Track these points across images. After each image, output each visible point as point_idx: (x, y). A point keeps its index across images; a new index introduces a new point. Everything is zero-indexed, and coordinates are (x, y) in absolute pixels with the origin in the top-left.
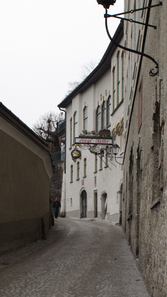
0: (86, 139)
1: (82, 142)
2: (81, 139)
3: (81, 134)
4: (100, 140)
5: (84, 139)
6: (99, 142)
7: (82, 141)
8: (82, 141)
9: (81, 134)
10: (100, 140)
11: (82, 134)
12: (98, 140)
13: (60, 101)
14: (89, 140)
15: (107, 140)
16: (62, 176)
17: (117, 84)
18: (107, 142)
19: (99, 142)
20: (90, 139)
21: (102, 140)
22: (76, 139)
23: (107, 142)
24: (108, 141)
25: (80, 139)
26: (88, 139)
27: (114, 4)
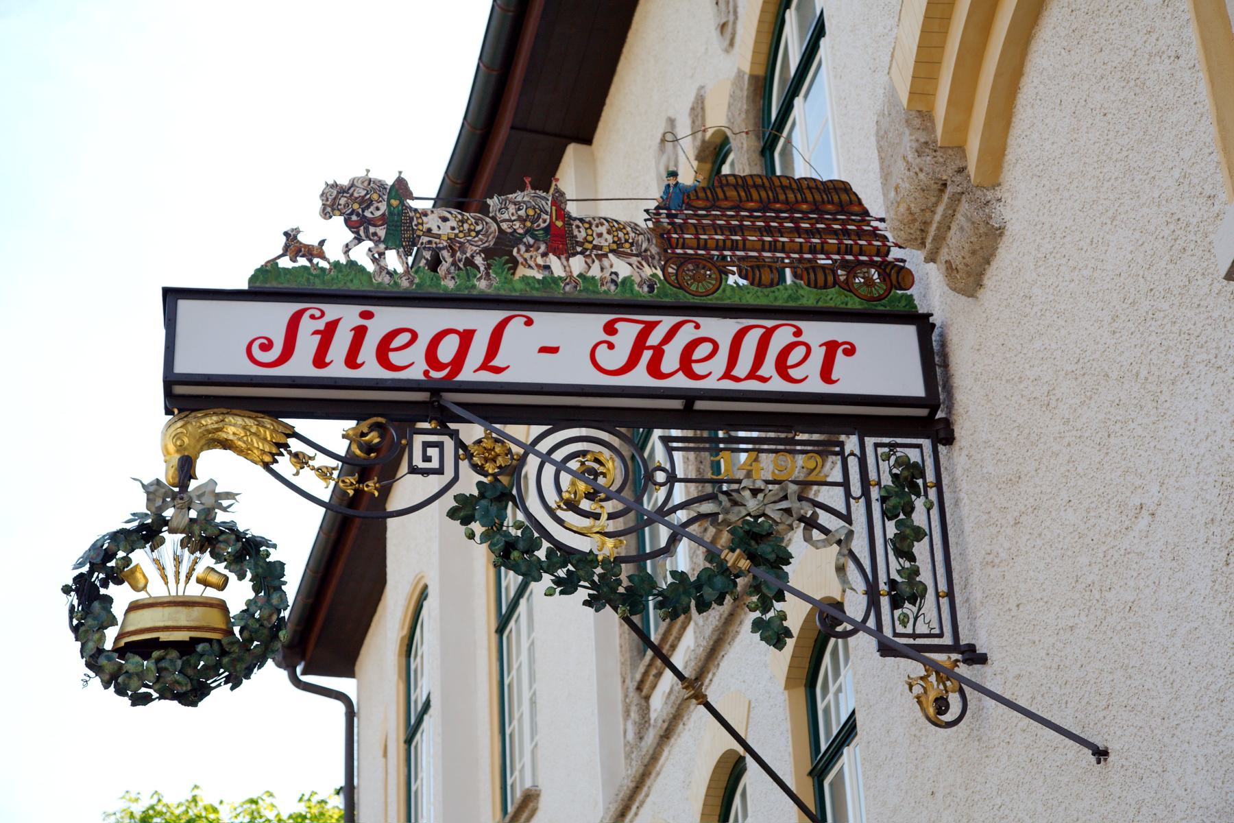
0: (386, 319)
1: (320, 360)
2: (286, 310)
3: (291, 237)
4: (676, 336)
5: (349, 315)
6: (670, 361)
7: (307, 343)
8: (307, 343)
9: (293, 245)
10: (687, 334)
11: (305, 238)
12: (628, 332)
13: (476, 335)
14: (467, 337)
15: (817, 332)
16: (447, 180)
17: (402, 738)
18: (826, 375)
19: (670, 361)
20: (483, 321)
21: (722, 329)
22: (183, 305)
23: (826, 375)
24: (831, 347)
25: (272, 318)
26: (428, 321)
27: (390, 181)
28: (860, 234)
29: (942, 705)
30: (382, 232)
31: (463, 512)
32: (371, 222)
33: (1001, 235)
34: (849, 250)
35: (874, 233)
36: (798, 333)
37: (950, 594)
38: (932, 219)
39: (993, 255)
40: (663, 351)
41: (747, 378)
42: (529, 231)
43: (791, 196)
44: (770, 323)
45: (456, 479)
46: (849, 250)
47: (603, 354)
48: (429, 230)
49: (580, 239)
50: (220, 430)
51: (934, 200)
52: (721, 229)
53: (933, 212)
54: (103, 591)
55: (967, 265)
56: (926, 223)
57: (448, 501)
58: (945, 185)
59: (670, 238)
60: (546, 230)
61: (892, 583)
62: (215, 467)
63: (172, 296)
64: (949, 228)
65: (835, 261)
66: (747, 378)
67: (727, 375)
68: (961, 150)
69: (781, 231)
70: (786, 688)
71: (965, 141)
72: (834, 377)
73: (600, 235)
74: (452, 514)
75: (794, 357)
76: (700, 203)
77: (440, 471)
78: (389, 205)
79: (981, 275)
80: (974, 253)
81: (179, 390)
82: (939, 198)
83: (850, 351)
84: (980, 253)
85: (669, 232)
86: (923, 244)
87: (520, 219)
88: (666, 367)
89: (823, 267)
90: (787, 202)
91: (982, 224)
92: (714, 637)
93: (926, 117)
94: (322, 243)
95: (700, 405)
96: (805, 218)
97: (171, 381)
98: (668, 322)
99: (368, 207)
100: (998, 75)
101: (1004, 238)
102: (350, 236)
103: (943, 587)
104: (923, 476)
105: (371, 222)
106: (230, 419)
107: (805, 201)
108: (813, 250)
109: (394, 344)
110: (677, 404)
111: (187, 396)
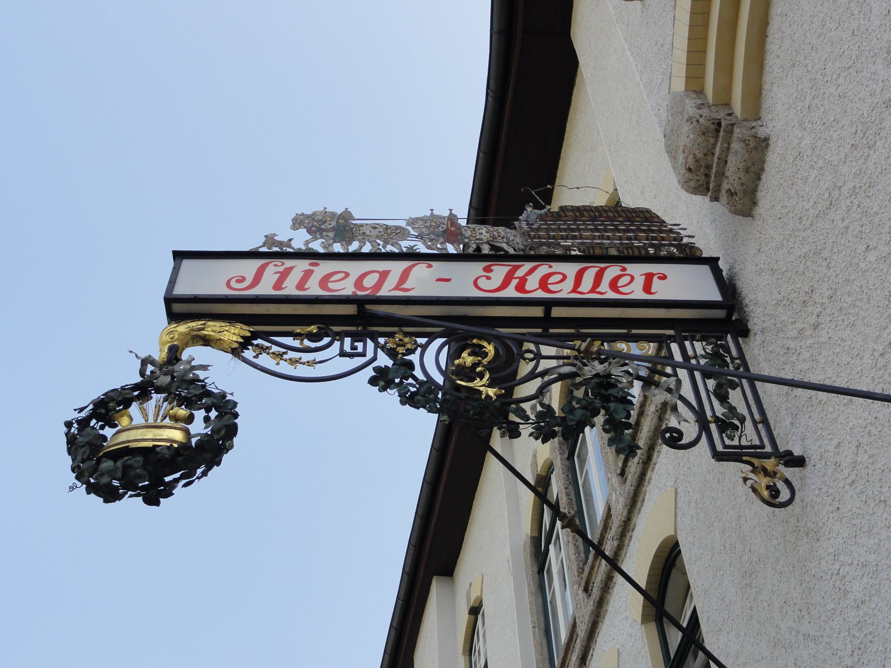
18: (647, 288)
22: (186, 264)
24: (649, 277)
28: (661, 231)
29: (774, 492)
30: (331, 234)
31: (382, 380)
32: (326, 230)
33: (767, 145)
34: (654, 239)
35: (671, 231)
36: (624, 269)
37: (765, 421)
38: (713, 160)
39: (762, 169)
40: (526, 280)
41: (589, 292)
42: (433, 233)
43: (610, 214)
44: (603, 265)
45: (374, 359)
46: (654, 239)
47: (482, 283)
48: (364, 233)
49: (467, 235)
50: (203, 329)
51: (712, 140)
52: (565, 230)
53: (713, 154)
54: (101, 432)
55: (742, 184)
56: (709, 167)
57: (369, 372)
58: (719, 124)
59: (529, 235)
60: (445, 231)
61: (717, 420)
62: (196, 354)
63: (179, 256)
64: (726, 162)
65: (645, 244)
66: (589, 292)
67: (574, 290)
68: (728, 104)
69: (606, 231)
70: (643, 622)
71: (730, 99)
72: (653, 291)
73: (481, 234)
74: (373, 381)
75: (621, 282)
76: (549, 218)
77: (363, 354)
78: (337, 222)
79: (754, 191)
80: (747, 171)
81: (177, 308)
82: (717, 137)
83: (663, 277)
84: (752, 169)
85: (528, 232)
86: (708, 189)
87: (426, 227)
88: (528, 287)
89: (638, 247)
90: (608, 217)
91: (752, 139)
92: (592, 620)
93: (700, 92)
94: (291, 240)
95: (556, 312)
96: (622, 223)
97: (169, 301)
98: (528, 266)
99: (323, 223)
100: (744, 81)
101: (771, 148)
102: (309, 237)
103: (757, 417)
104: (728, 351)
105: (326, 230)
106: (210, 323)
107: (621, 216)
108: (629, 238)
109: (331, 279)
110: (537, 312)
111: (178, 308)
